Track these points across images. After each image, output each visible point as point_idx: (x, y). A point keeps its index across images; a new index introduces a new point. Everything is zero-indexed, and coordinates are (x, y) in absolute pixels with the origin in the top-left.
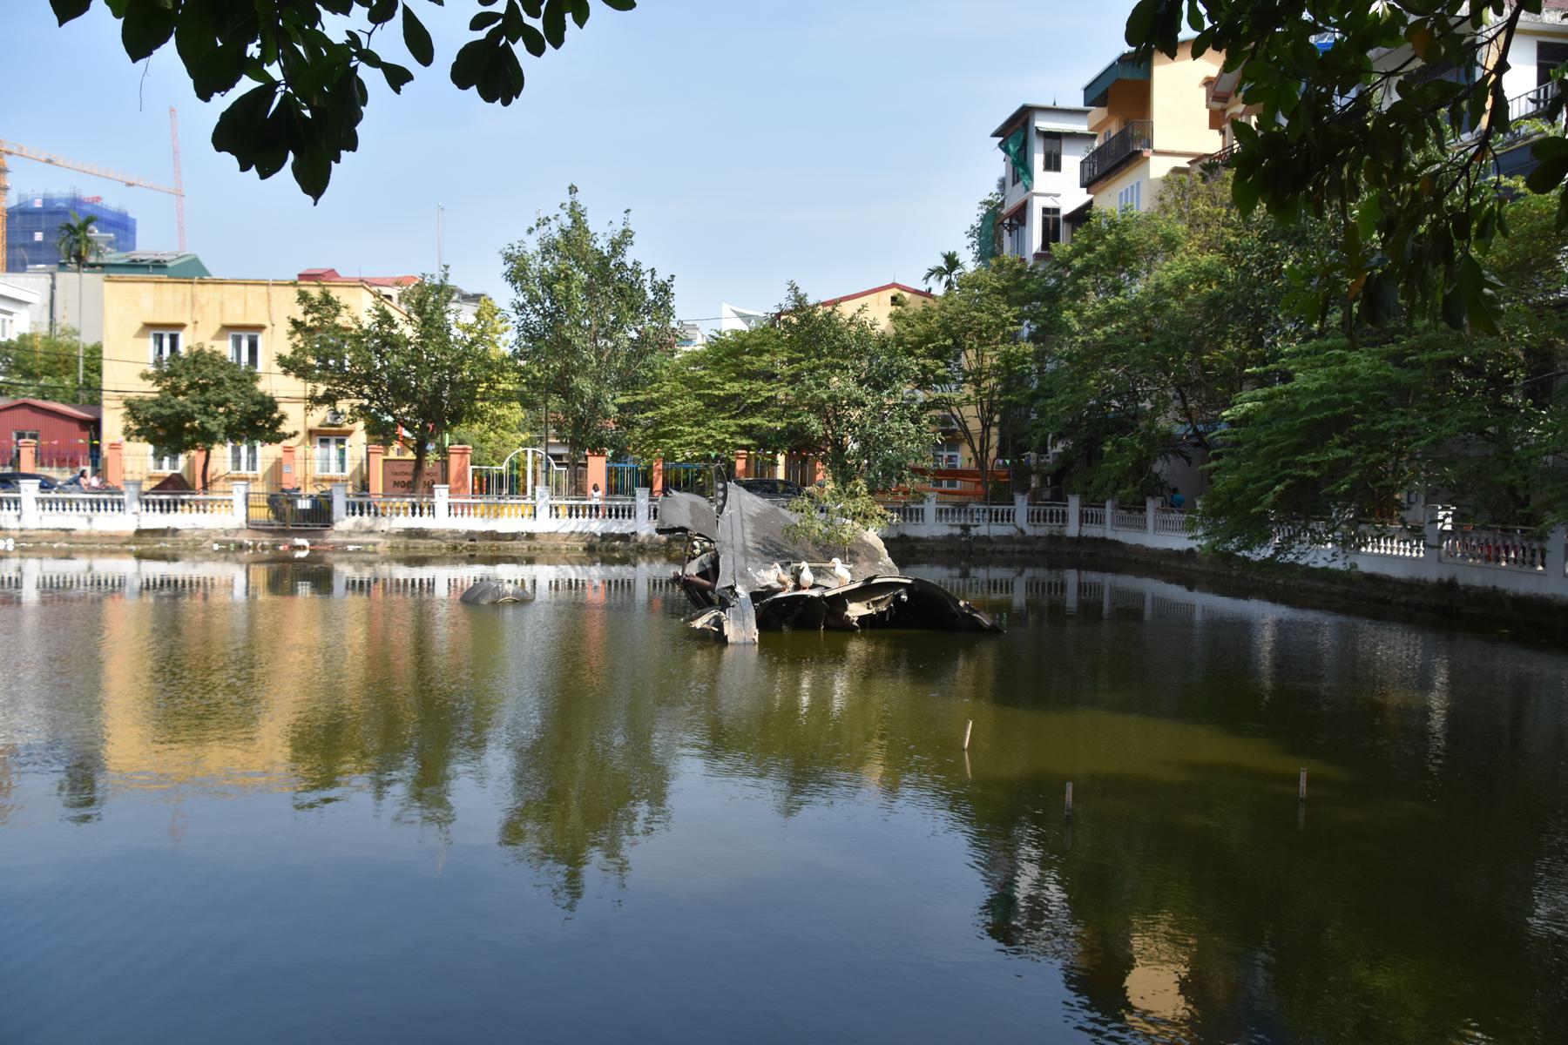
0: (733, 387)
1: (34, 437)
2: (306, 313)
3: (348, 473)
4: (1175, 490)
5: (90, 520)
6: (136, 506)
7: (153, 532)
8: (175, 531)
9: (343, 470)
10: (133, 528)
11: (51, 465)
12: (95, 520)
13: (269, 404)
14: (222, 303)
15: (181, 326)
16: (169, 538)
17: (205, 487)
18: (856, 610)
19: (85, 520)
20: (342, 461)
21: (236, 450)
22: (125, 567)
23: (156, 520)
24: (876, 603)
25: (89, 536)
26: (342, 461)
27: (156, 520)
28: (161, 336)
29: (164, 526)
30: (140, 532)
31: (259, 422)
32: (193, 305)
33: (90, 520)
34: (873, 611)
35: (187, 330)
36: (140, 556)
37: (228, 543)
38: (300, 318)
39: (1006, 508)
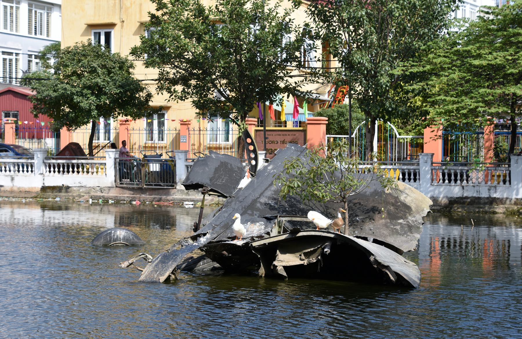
0: (498, 58)
1: (15, 116)
2: (158, 10)
3: (230, 142)
4: (165, 147)
5: (12, 179)
6: (43, 169)
7: (53, 188)
8: (68, 187)
9: (227, 139)
10: (40, 186)
11: (24, 138)
12: (16, 178)
13: (137, 86)
14: (141, 5)
15: (112, 25)
16: (63, 194)
17: (91, 153)
18: (285, 260)
19: (9, 179)
20: (161, 132)
21: (150, 125)
22: (35, 215)
23: (56, 179)
24: (308, 255)
25: (12, 192)
26: (161, 132)
27: (56, 179)
28: (99, 34)
29: (60, 184)
30: (44, 189)
31: (130, 101)
32: (121, 8)
33: (12, 179)
34: (306, 262)
35: (117, 28)
36: (44, 207)
37: (99, 198)
38: (154, 12)
39: (30, 161)
